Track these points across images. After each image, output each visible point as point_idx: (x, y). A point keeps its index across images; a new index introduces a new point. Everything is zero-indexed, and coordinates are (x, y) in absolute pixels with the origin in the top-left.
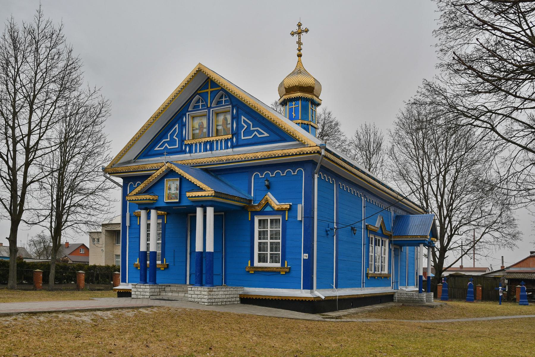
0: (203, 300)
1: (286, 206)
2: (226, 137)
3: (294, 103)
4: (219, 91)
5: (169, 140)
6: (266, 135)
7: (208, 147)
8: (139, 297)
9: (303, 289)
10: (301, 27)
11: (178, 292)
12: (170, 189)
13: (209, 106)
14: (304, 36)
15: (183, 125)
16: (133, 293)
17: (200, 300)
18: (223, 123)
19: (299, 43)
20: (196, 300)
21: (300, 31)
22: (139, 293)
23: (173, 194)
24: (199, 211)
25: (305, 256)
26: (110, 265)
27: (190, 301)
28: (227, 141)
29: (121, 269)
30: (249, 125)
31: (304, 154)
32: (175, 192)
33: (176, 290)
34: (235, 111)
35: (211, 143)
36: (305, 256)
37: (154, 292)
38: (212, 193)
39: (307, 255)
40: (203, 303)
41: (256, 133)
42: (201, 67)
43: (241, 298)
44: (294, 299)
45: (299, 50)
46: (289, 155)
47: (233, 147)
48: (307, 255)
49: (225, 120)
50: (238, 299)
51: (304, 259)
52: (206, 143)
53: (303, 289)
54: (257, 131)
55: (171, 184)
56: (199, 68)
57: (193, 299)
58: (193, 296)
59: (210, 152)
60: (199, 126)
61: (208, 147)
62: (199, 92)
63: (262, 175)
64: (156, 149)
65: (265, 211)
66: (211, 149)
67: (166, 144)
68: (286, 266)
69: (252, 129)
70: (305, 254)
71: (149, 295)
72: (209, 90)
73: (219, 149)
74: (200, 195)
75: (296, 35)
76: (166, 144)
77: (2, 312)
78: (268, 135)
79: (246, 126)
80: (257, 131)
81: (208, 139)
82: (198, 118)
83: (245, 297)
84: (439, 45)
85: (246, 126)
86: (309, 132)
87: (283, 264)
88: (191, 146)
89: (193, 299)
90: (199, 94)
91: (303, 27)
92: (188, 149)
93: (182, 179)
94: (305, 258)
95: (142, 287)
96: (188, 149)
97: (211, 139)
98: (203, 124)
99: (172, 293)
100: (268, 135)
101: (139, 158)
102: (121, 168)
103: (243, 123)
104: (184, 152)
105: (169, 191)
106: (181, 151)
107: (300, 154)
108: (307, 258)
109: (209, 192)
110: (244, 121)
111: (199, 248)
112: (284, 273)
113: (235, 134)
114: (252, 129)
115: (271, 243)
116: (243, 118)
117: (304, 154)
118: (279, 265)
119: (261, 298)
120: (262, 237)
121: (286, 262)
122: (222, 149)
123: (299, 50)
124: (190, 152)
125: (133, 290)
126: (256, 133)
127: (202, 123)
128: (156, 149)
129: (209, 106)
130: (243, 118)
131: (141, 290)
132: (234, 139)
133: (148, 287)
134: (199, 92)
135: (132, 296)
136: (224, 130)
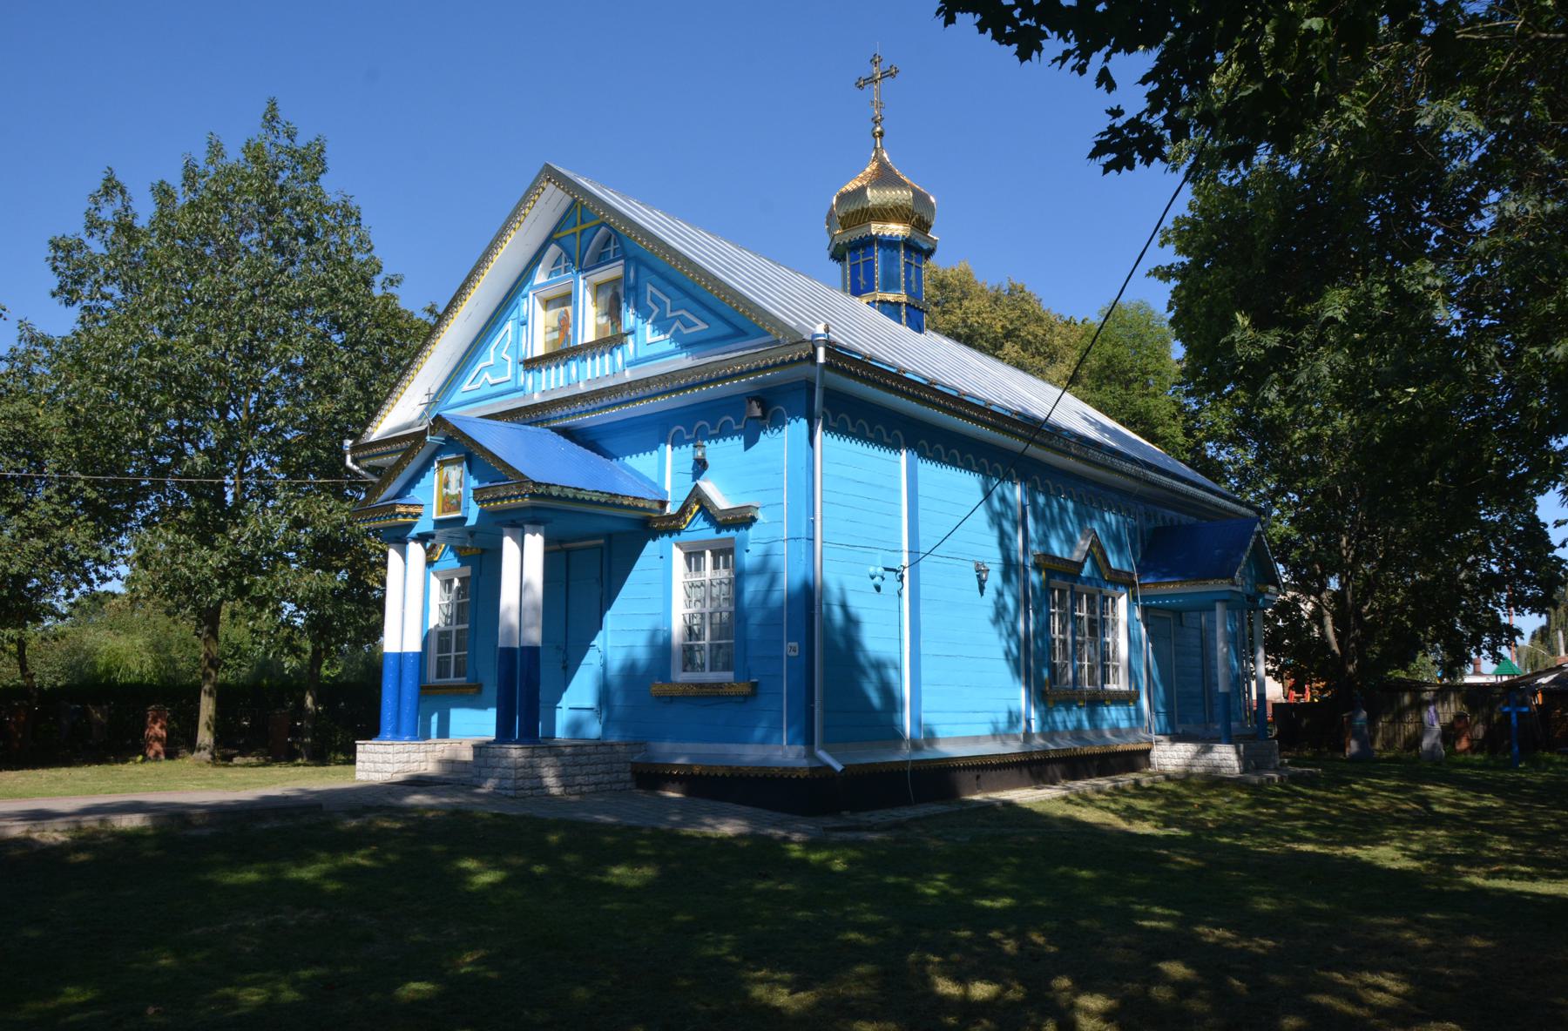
3: (861, 252)
4: (600, 226)
6: (702, 326)
22: (372, 765)
26: (941, 732)
37: (408, 762)
43: (634, 773)
50: (628, 776)
67: (487, 375)
69: (669, 315)
76: (487, 375)
77: (1566, 880)
79: (657, 311)
83: (712, 774)
85: (657, 311)
86: (901, 323)
90: (558, 242)
94: (792, 654)
103: (649, 302)
105: (445, 490)
108: (796, 654)
110: (655, 300)
114: (669, 315)
116: (650, 288)
126: (677, 324)
127: (566, 312)
130: (650, 288)
131: (379, 758)
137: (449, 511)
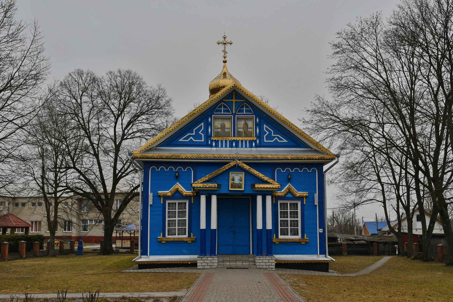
0: (271, 267)
1: (305, 194)
2: (251, 139)
4: (244, 102)
5: (194, 134)
6: (285, 141)
7: (234, 144)
8: (206, 267)
9: (320, 254)
10: (226, 39)
11: (236, 261)
12: (233, 180)
13: (234, 113)
14: (228, 47)
15: (208, 124)
16: (198, 264)
17: (268, 266)
18: (244, 126)
19: (225, 52)
20: (264, 267)
21: (225, 42)
23: (237, 184)
24: (259, 199)
25: (321, 231)
27: (259, 268)
28: (251, 142)
29: (139, 244)
30: (270, 132)
31: (324, 159)
32: (238, 183)
33: (228, 259)
34: (258, 120)
35: (237, 142)
36: (321, 231)
38: (279, 187)
39: (322, 229)
40: (271, 269)
41: (276, 138)
42: (237, 84)
44: (315, 262)
45: (225, 57)
46: (313, 159)
47: (256, 146)
48: (322, 229)
49: (245, 124)
51: (319, 233)
52: (231, 142)
53: (320, 254)
54: (278, 137)
55: (234, 176)
56: (234, 85)
57: (261, 267)
58: (261, 264)
59: (235, 149)
60: (221, 126)
61: (234, 144)
62: (224, 100)
63: (283, 170)
64: (181, 140)
65: (287, 197)
66: (237, 146)
68: (305, 238)
70: (320, 229)
71: (217, 265)
72: (234, 100)
73: (244, 146)
74: (268, 187)
75: (222, 44)
78: (203, 123)
79: (268, 133)
80: (278, 137)
81: (233, 138)
82: (220, 120)
84: (328, 72)
85: (268, 133)
87: (189, 235)
88: (217, 142)
89: (261, 267)
91: (228, 40)
92: (214, 144)
93: (247, 173)
94: (321, 232)
95: (209, 259)
96: (214, 144)
97: (238, 139)
98: (225, 125)
99: (230, 262)
100: (203, 123)
101: (162, 146)
102: (152, 154)
104: (211, 146)
105: (232, 182)
106: (207, 145)
107: (321, 159)
109: (276, 185)
110: (266, 129)
111: (259, 226)
112: (165, 242)
113: (259, 137)
114: (273, 135)
115: (290, 220)
116: (265, 126)
117: (324, 159)
118: (299, 237)
119: (289, 262)
120: (282, 216)
121: (305, 235)
122: (243, 147)
123: (225, 57)
124: (217, 146)
125: (198, 261)
126: (276, 138)
128: (181, 140)
129: (234, 113)
130: (265, 126)
132: (258, 141)
133: (216, 259)
134: (224, 100)
135: (198, 267)
136: (245, 132)
137: (235, 188)
